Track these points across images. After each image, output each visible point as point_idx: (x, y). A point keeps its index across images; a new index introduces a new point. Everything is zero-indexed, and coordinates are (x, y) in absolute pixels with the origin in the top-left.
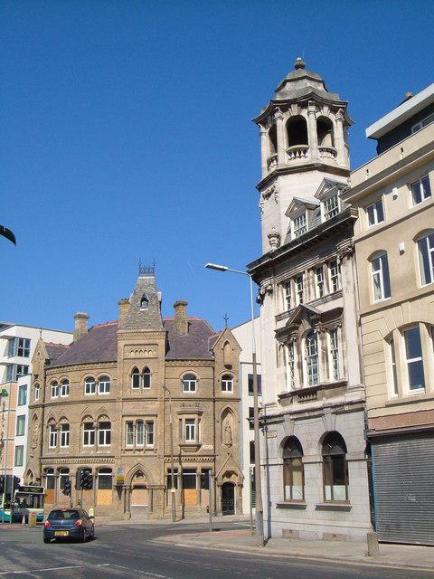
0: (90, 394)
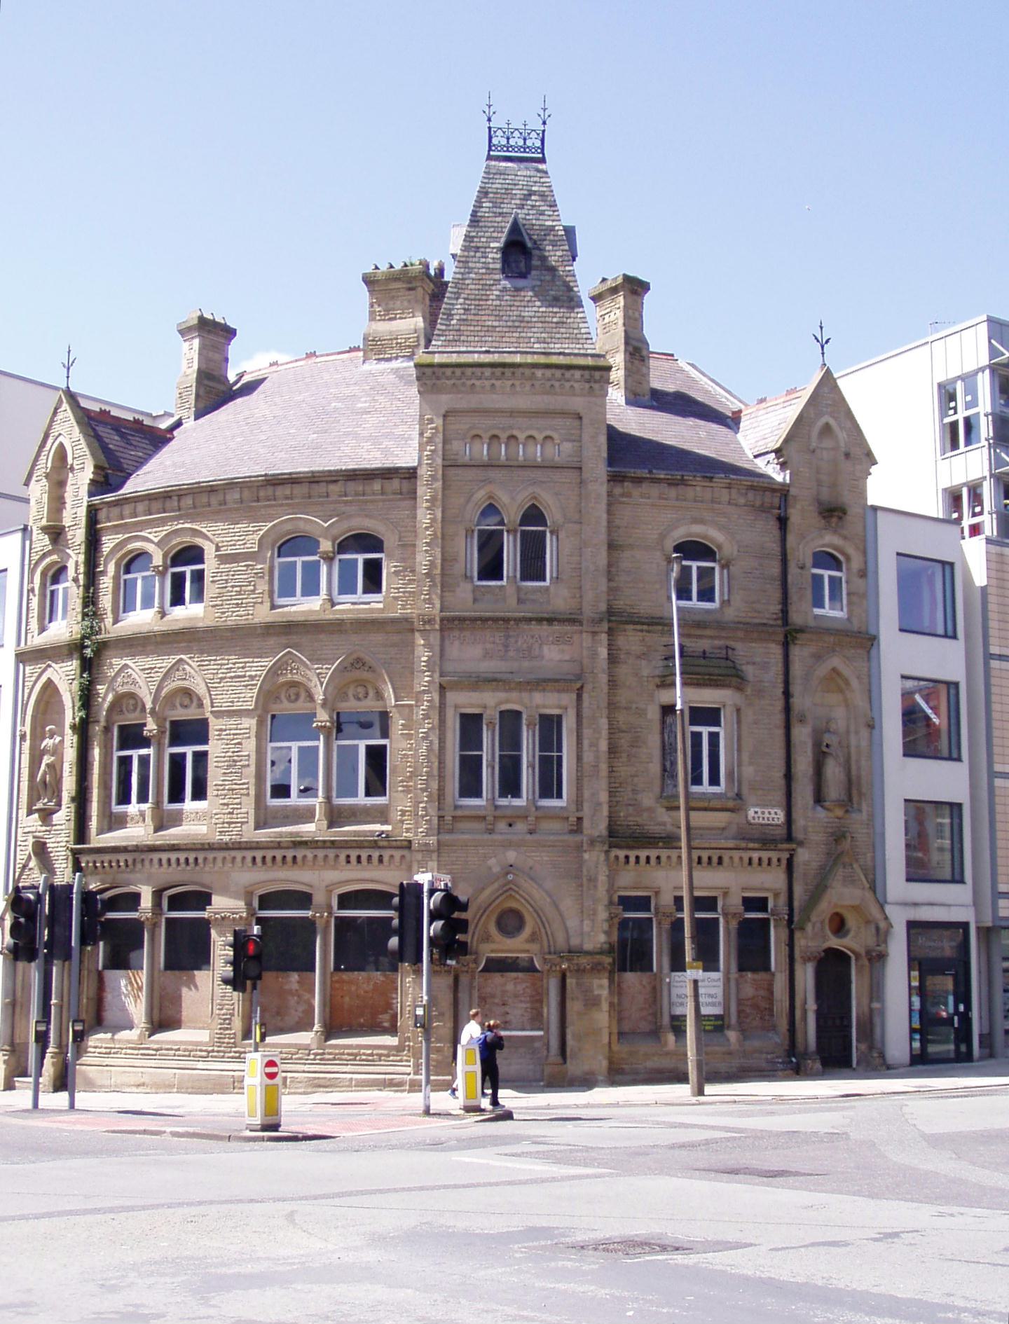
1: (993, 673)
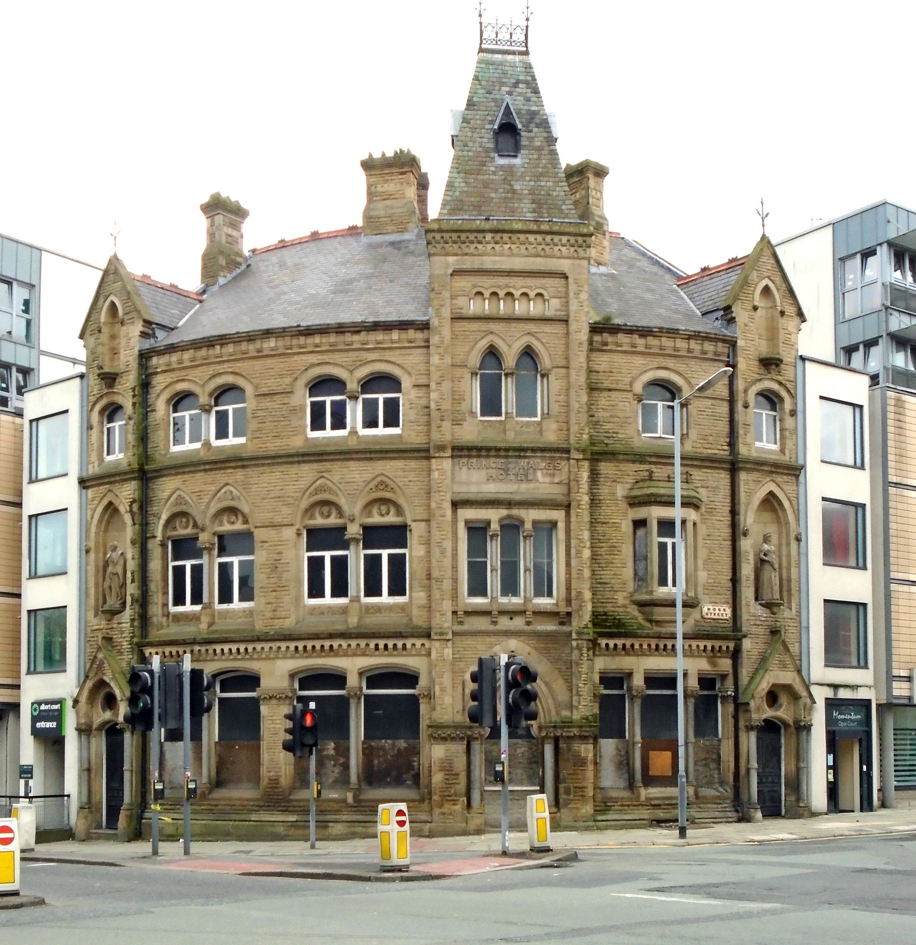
0: (328, 433)
1: (891, 497)
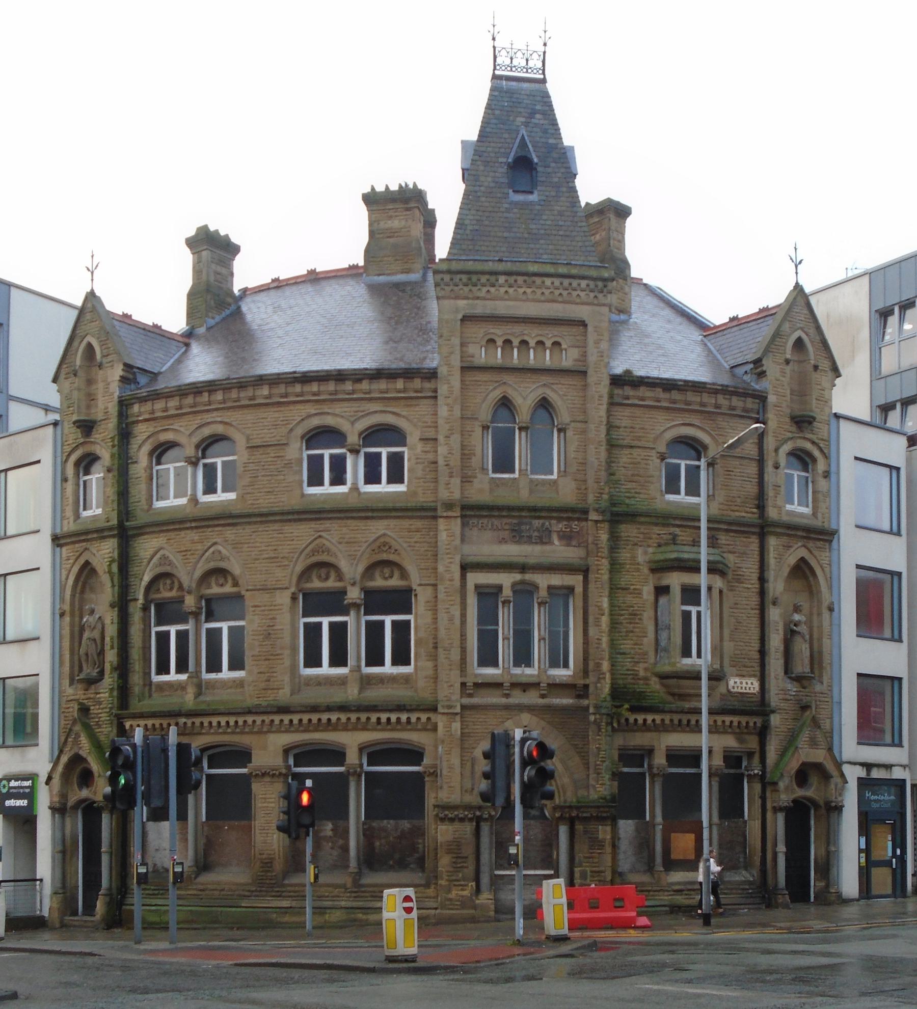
0: (327, 489)
